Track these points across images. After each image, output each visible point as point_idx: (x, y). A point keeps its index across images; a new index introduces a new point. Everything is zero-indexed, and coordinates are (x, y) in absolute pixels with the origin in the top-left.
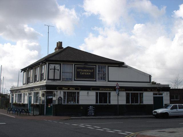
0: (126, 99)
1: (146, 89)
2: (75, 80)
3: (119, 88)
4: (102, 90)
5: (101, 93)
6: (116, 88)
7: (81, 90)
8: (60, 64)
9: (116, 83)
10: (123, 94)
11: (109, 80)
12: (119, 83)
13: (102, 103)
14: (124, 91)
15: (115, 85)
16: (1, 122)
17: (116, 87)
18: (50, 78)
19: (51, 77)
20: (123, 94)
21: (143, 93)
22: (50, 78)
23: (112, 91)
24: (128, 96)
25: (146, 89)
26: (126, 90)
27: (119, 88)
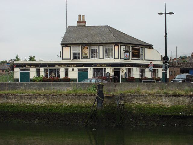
0: (68, 73)
1: (31, 65)
2: (82, 59)
3: (152, 65)
4: (57, 67)
5: (98, 68)
6: (150, 65)
7: (31, 67)
8: (103, 46)
9: (150, 62)
10: (76, 69)
11: (63, 58)
12: (152, 62)
13: (169, 74)
14: (34, 67)
15: (149, 63)
16: (2, 90)
17: (149, 64)
18: (121, 57)
19: (122, 57)
20: (76, 69)
21: (60, 69)
22: (100, 57)
23: (146, 67)
24: (46, 70)
25: (31, 65)
26: (77, 66)
27: (152, 65)
